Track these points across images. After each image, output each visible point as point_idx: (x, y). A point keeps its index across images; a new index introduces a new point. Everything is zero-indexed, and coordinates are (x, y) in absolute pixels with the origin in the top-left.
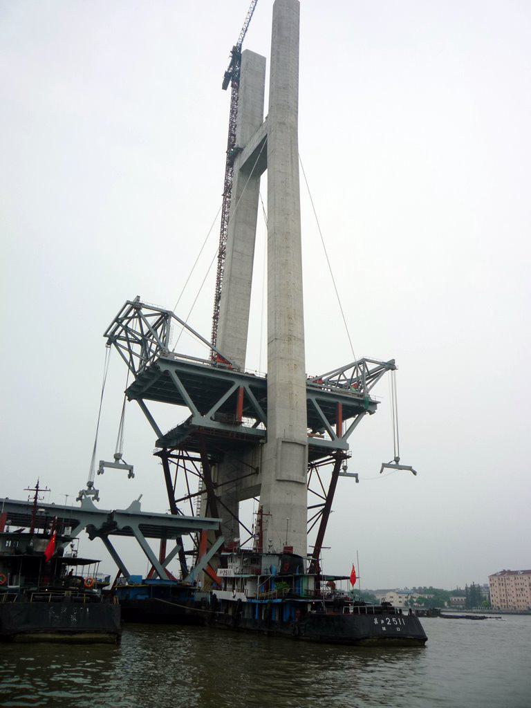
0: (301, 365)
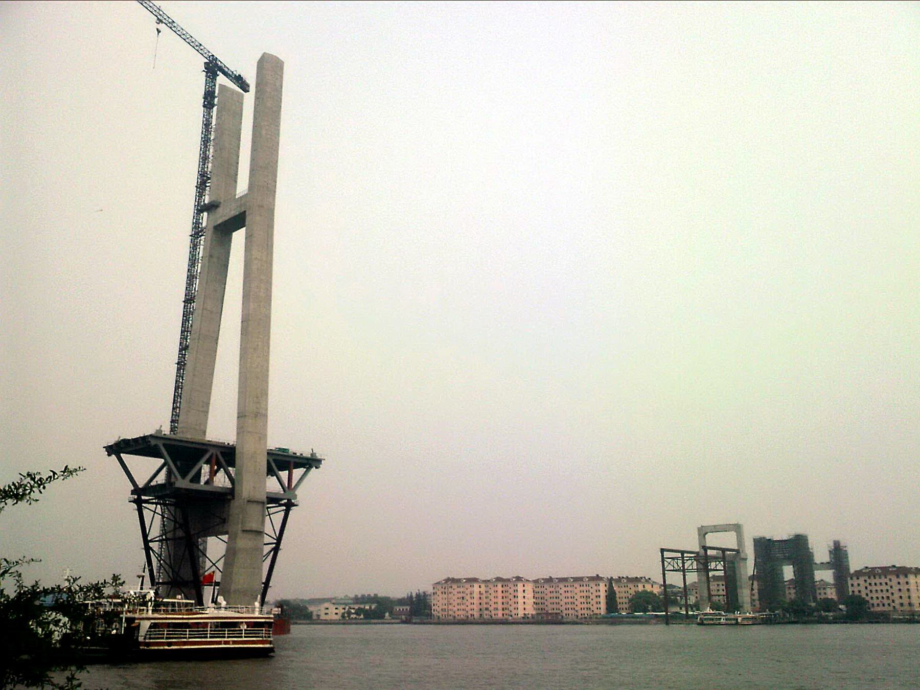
0: (263, 437)
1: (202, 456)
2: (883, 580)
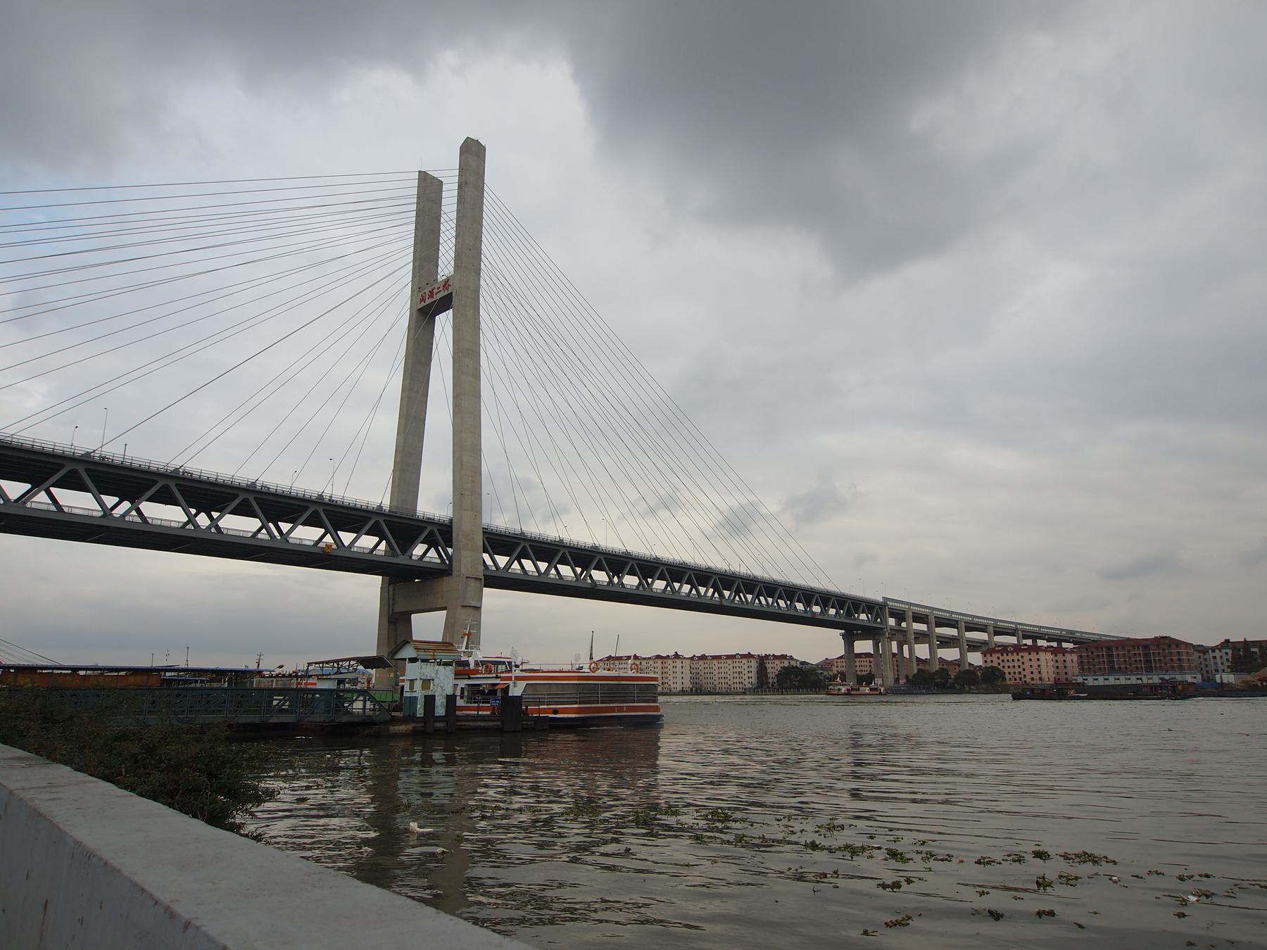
1: (420, 534)
2: (1016, 657)
